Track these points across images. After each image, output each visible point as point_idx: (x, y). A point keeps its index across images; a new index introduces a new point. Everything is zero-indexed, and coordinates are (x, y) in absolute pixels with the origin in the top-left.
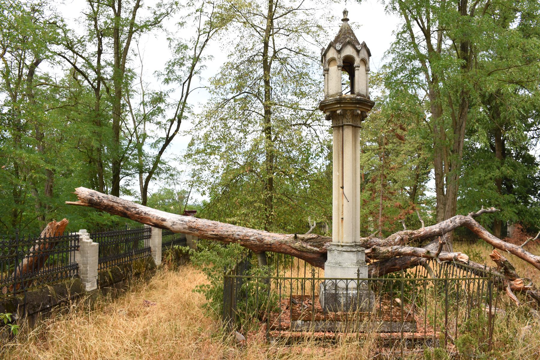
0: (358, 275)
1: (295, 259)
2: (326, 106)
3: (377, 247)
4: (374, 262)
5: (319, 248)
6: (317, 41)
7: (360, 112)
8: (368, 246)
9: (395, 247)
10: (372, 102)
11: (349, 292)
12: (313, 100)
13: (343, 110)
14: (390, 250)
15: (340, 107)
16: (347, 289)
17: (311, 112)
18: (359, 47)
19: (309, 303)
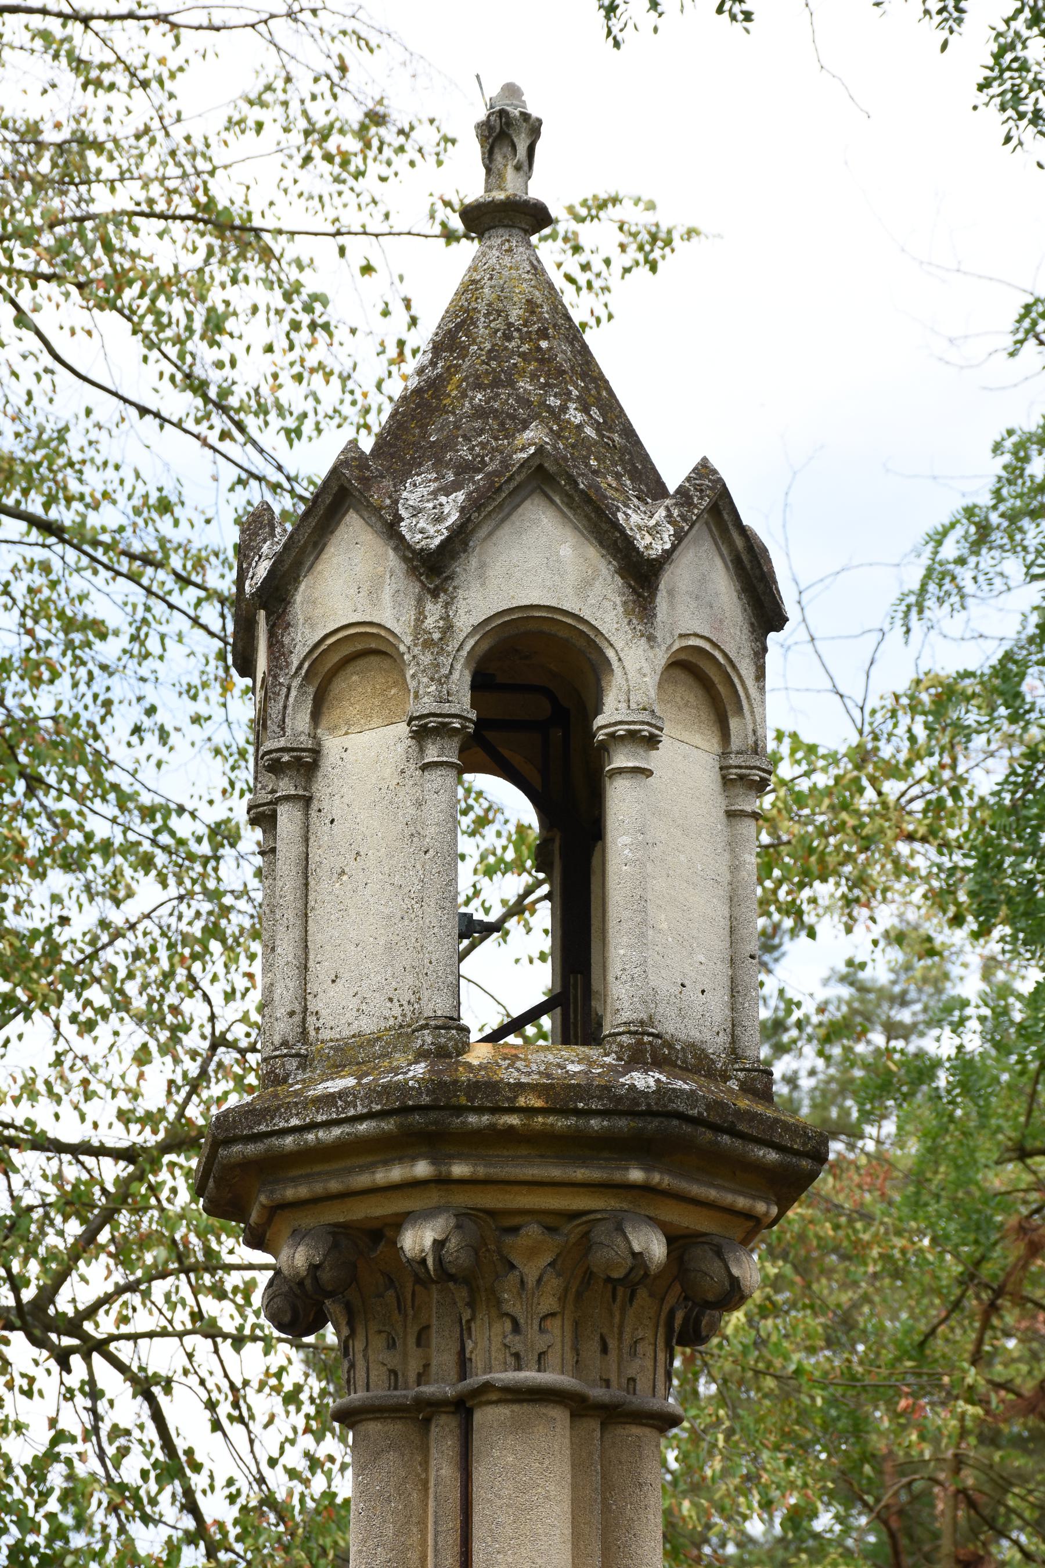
2: (275, 1166)
6: (197, 386)
7: (655, 1247)
10: (798, 1130)
12: (133, 1036)
13: (464, 1218)
15: (442, 1182)
17: (111, 1171)
18: (648, 527)
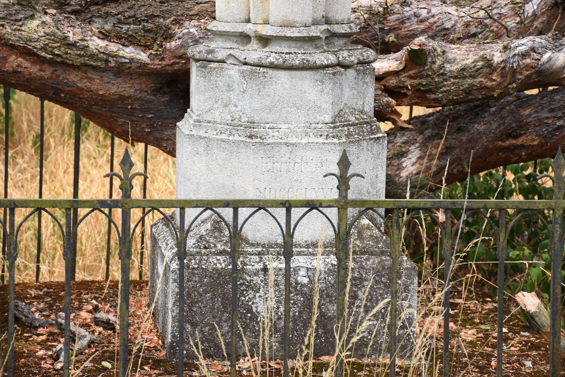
0: (343, 182)
1: (24, 104)
3: (432, 44)
4: (411, 120)
5: (145, 47)
8: (391, 38)
9: (524, 44)
11: (298, 261)
14: (497, 58)
16: (287, 249)
19: (97, 322)
